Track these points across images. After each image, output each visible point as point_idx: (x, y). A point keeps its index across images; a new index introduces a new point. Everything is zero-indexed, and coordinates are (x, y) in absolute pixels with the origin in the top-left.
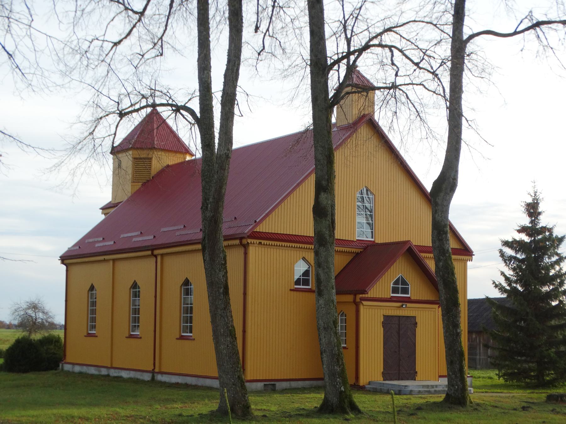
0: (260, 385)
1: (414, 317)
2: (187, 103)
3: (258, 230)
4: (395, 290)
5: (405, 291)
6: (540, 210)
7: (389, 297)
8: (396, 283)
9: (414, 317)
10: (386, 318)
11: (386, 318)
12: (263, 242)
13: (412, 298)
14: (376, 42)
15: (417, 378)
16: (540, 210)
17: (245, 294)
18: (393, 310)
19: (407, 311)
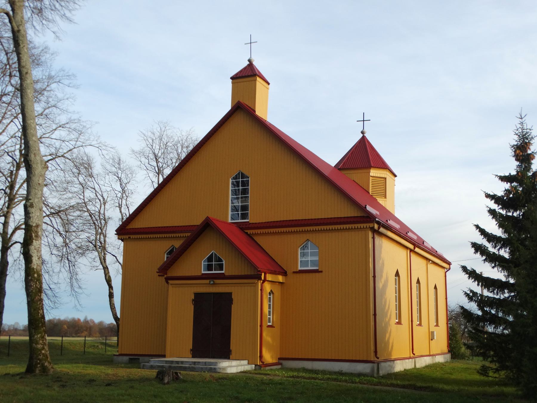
0: (126, 358)
1: (230, 294)
2: (65, 153)
3: (131, 227)
4: (209, 268)
5: (221, 267)
6: (330, 152)
7: (200, 274)
8: (210, 259)
9: (230, 294)
10: (196, 295)
11: (196, 295)
12: (132, 236)
13: (227, 274)
14: (47, 135)
15: (231, 356)
16: (330, 152)
17: (446, 299)
18: (205, 288)
19: (221, 288)
